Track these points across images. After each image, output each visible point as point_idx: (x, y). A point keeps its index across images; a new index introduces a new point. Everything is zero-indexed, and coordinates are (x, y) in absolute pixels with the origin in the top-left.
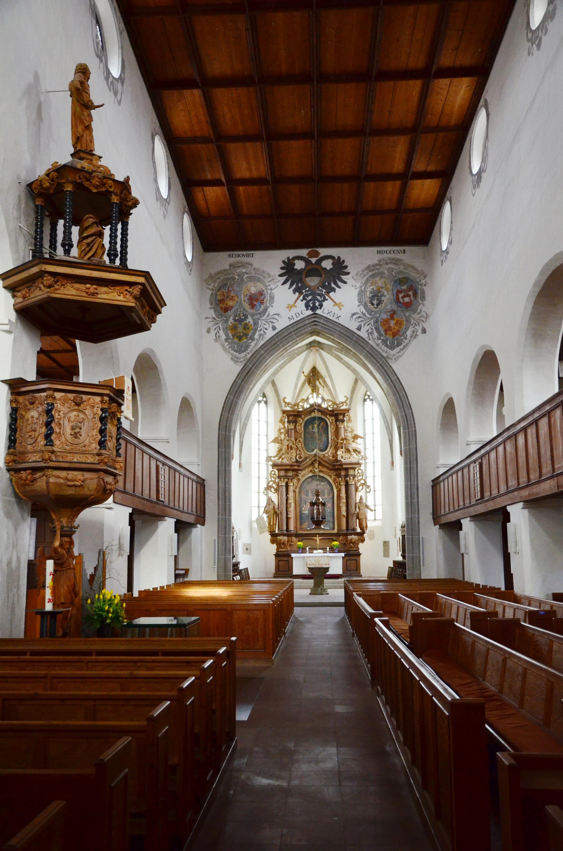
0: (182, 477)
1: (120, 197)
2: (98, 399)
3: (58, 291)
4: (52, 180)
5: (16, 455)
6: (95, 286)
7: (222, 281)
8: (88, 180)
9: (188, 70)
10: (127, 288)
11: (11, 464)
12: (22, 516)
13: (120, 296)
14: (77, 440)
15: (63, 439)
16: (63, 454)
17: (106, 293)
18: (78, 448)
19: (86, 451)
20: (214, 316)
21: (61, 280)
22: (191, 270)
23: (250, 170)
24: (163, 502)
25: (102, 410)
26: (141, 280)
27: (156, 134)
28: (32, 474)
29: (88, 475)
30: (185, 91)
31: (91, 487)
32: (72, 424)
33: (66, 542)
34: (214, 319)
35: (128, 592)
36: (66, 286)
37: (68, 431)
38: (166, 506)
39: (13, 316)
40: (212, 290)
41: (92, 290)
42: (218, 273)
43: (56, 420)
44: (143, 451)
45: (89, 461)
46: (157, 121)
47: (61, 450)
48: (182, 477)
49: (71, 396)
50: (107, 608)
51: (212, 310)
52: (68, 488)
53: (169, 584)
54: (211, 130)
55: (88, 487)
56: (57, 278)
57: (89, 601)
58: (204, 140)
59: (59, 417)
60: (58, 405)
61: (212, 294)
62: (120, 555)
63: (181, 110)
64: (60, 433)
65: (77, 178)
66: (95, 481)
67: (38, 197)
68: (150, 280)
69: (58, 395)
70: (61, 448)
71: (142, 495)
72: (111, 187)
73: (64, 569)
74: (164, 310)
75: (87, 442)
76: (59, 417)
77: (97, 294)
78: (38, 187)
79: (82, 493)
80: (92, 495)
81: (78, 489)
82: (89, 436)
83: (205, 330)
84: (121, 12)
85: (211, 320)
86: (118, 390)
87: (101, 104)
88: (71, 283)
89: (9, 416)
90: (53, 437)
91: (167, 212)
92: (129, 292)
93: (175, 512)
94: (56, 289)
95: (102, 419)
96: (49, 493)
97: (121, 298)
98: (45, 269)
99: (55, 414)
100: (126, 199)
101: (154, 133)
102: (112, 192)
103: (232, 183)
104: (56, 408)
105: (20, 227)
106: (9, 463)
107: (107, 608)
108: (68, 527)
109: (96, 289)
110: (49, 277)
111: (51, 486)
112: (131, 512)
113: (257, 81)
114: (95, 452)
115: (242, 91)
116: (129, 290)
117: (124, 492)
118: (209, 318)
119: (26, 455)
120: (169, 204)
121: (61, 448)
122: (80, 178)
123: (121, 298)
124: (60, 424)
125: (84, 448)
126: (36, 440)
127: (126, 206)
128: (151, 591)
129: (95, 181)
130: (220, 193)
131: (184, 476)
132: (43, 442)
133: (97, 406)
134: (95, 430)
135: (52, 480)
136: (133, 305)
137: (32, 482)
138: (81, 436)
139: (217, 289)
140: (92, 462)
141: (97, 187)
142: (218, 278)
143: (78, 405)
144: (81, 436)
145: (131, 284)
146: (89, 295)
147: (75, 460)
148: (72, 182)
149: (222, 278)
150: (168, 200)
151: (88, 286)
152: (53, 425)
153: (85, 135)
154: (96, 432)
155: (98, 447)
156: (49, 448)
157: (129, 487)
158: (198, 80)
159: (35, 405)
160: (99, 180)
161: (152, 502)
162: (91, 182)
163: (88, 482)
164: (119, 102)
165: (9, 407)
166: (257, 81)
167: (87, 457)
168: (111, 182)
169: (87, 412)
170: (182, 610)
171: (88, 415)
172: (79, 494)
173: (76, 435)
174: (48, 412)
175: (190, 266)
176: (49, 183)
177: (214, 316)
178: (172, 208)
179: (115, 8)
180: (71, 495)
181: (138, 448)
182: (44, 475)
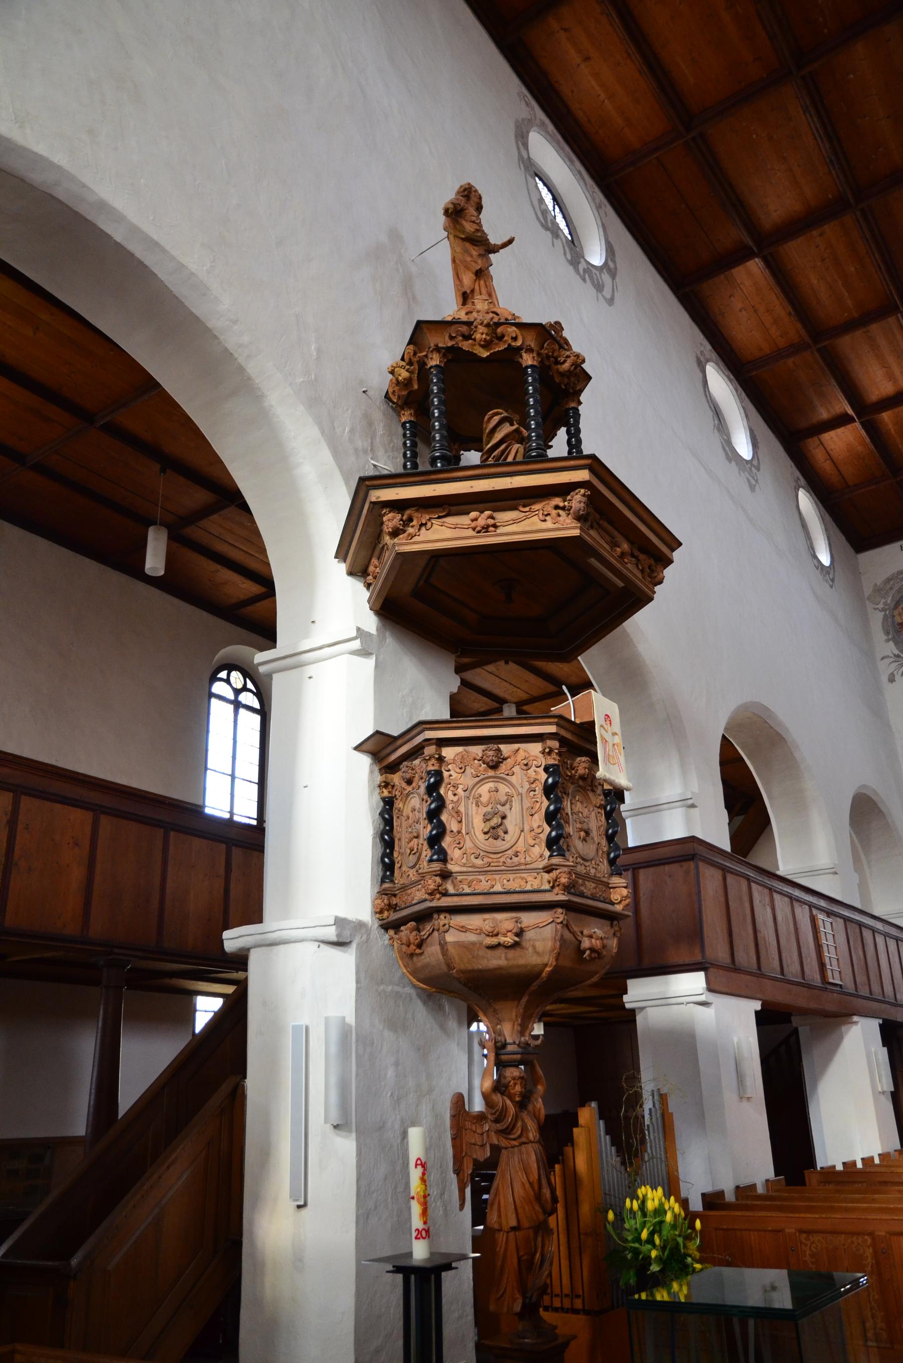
0: (880, 940)
1: (539, 354)
2: (535, 748)
3: (416, 539)
4: (410, 363)
5: (395, 895)
6: (488, 513)
7: (899, 591)
8: (467, 337)
9: (733, 234)
10: (558, 501)
11: (386, 914)
12: (443, 1027)
13: (545, 521)
14: (499, 842)
15: (468, 844)
16: (471, 878)
17: (515, 522)
18: (502, 860)
19: (520, 864)
20: (897, 652)
21: (416, 514)
22: (833, 580)
23: (891, 377)
24: (841, 986)
25: (546, 769)
26: (583, 475)
27: (708, 361)
28: (419, 931)
29: (528, 919)
30: (734, 271)
31: (539, 946)
32: (485, 810)
33: (514, 1079)
34: (898, 656)
35: (776, 1176)
36: (429, 525)
37: (478, 825)
38: (851, 995)
39: (371, 623)
40: (883, 610)
41: (482, 522)
42: (888, 580)
43: (450, 807)
44: (770, 889)
45: (529, 888)
46: (706, 343)
47: (465, 869)
48: (880, 940)
49: (477, 750)
50: (644, 1235)
51: (891, 644)
52: (490, 953)
53: (887, 1150)
54: (799, 326)
55: (534, 947)
56: (408, 512)
57: (611, 1216)
58: (794, 349)
59: (455, 799)
60: (451, 774)
61: (885, 615)
62: (742, 1097)
63: (740, 310)
64: (459, 832)
65: (447, 338)
66: (549, 932)
67: (403, 409)
68: (633, 503)
69: (448, 752)
70: (464, 865)
71: (782, 973)
72: (515, 339)
73: (515, 1143)
74: (676, 555)
75: (520, 846)
76: (455, 799)
77: (495, 526)
78: (396, 388)
79: (521, 962)
80: (546, 965)
81: (511, 953)
82: (527, 826)
83: (884, 678)
84: (592, 177)
85: (892, 660)
86: (581, 723)
87: (506, 239)
88: (439, 517)
89: (377, 816)
90: (447, 842)
91: (757, 481)
92: (563, 508)
93: (876, 1005)
94: (412, 536)
95: (548, 790)
96: (449, 966)
97: (549, 524)
98: (379, 497)
99: (446, 793)
100: (556, 358)
101: (702, 359)
102: (519, 349)
103: (866, 411)
104: (446, 780)
105: (375, 466)
106: (381, 912)
107: (644, 1235)
108: (514, 1043)
109: (492, 517)
110: (391, 515)
111: (452, 951)
112: (624, 996)
113: (852, 201)
114: (541, 864)
115: (830, 230)
116: (561, 504)
117: (733, 968)
118: (888, 657)
119: (409, 891)
120: (758, 470)
121: (464, 865)
122: (451, 338)
123: (549, 524)
124: (458, 812)
125: (515, 859)
126: (420, 855)
127: (562, 374)
128: (839, 1172)
129: (481, 334)
130: (852, 439)
131: (886, 935)
132: (427, 853)
133: (535, 762)
134: (536, 816)
135: (450, 938)
136: (576, 532)
137: (420, 946)
138: (506, 833)
139: (892, 606)
140: (535, 887)
141: (486, 345)
142: (891, 589)
143: (495, 767)
144: (506, 833)
145: (564, 490)
146: (479, 532)
147: (498, 888)
148: (437, 349)
149: (897, 587)
150: (755, 463)
151: (473, 514)
152: (444, 817)
153: (477, 287)
154: (539, 820)
155: (547, 853)
156: (437, 866)
157: (746, 957)
158: (751, 243)
159: (414, 784)
160: (485, 330)
161: (809, 987)
162: (475, 340)
163: (529, 935)
164: (611, 301)
165: (377, 798)
166: (852, 201)
167: (522, 878)
168: (514, 328)
169: (513, 779)
170: (858, 1234)
171: (518, 786)
172: (519, 966)
173: (495, 832)
174: (433, 789)
175: (828, 573)
176: (407, 370)
177: (897, 652)
178: (766, 476)
179: (580, 173)
180: (500, 968)
181: (755, 882)
182: (433, 930)
